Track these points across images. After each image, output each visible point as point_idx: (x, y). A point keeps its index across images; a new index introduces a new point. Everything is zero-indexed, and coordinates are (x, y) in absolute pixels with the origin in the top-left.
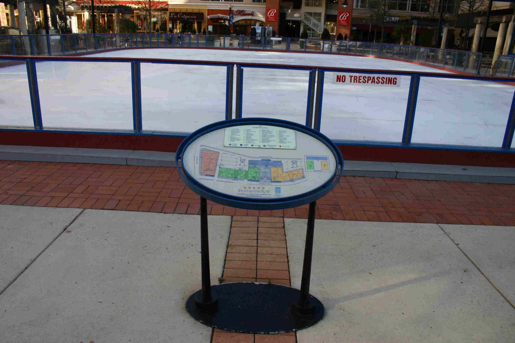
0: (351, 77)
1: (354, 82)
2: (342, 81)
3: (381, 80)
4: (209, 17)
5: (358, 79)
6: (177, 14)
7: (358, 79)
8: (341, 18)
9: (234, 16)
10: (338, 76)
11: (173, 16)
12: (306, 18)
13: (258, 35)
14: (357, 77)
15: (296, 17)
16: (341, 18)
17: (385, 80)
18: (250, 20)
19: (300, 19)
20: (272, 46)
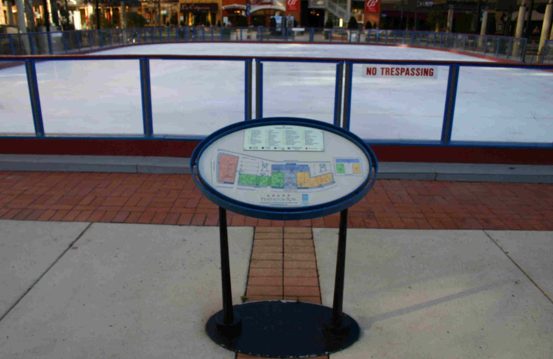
0: (383, 69)
1: (386, 74)
2: (373, 74)
3: (415, 72)
4: (223, 8)
5: (390, 71)
6: (188, 5)
7: (390, 71)
8: (370, 4)
9: (252, 6)
10: (368, 69)
11: (185, 7)
12: (331, 6)
13: (278, 26)
14: (389, 69)
15: (319, 5)
16: (370, 4)
17: (420, 72)
18: (270, 9)
19: (323, 7)
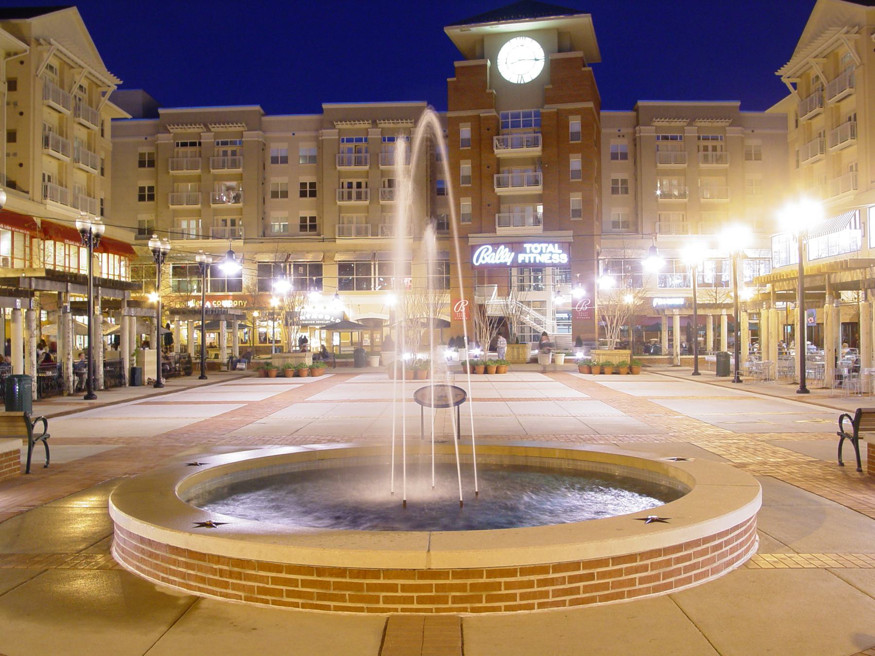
20: (495, 231)
